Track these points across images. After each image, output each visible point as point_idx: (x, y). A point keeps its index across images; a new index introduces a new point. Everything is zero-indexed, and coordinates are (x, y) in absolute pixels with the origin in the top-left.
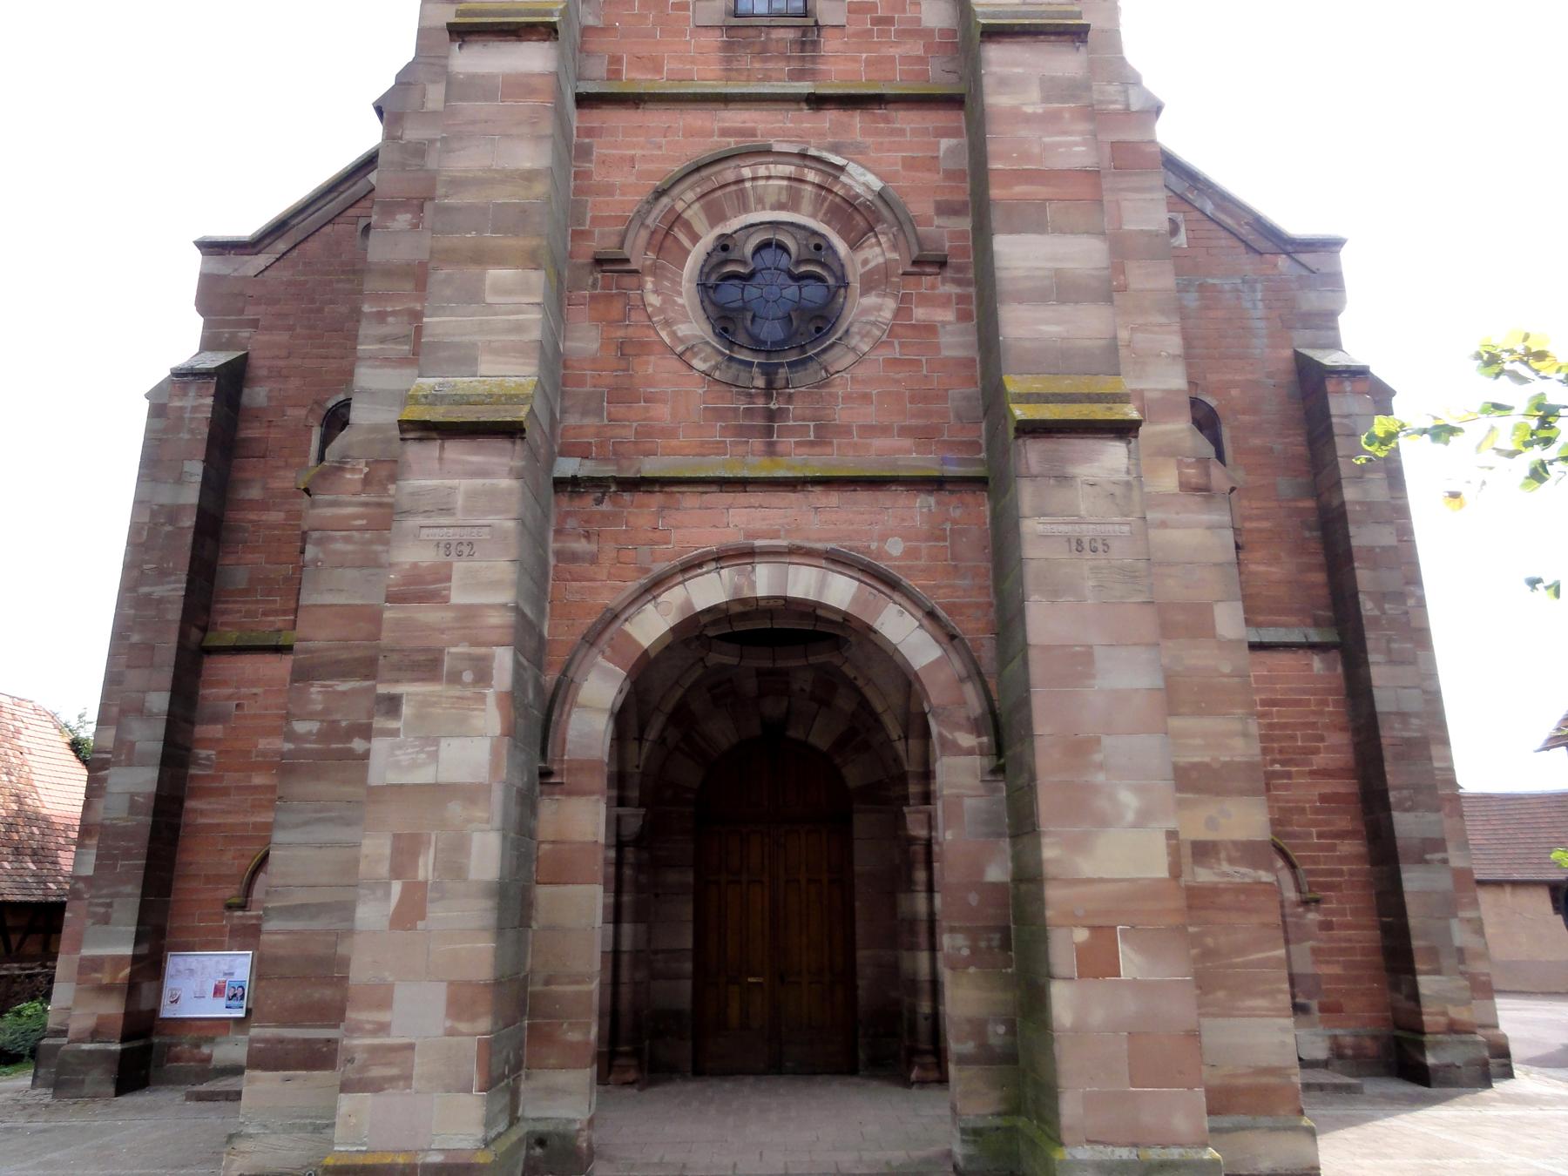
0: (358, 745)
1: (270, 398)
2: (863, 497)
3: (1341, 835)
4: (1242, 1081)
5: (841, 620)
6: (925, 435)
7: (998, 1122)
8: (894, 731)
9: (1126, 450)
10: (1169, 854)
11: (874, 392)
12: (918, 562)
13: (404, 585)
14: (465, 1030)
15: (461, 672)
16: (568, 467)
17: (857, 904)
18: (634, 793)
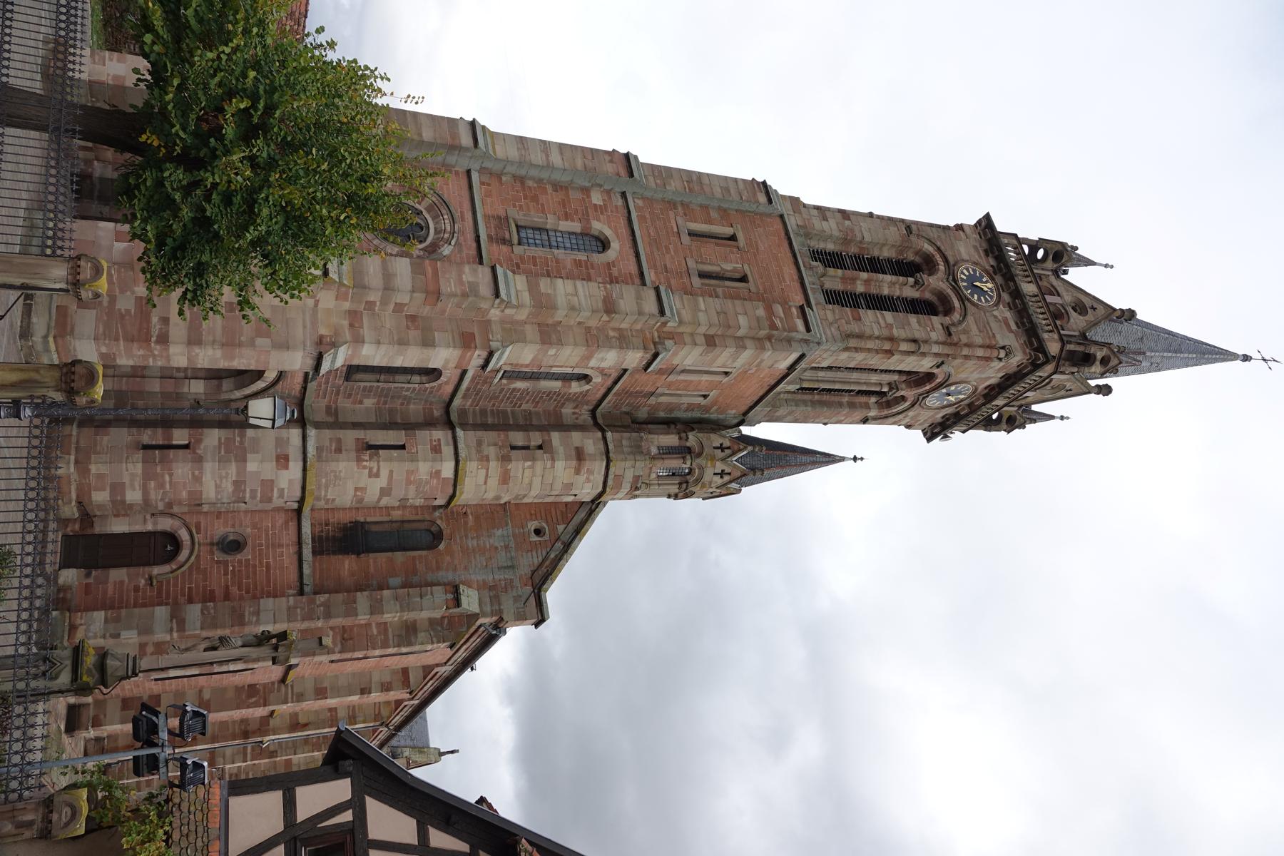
4: (69, 319)
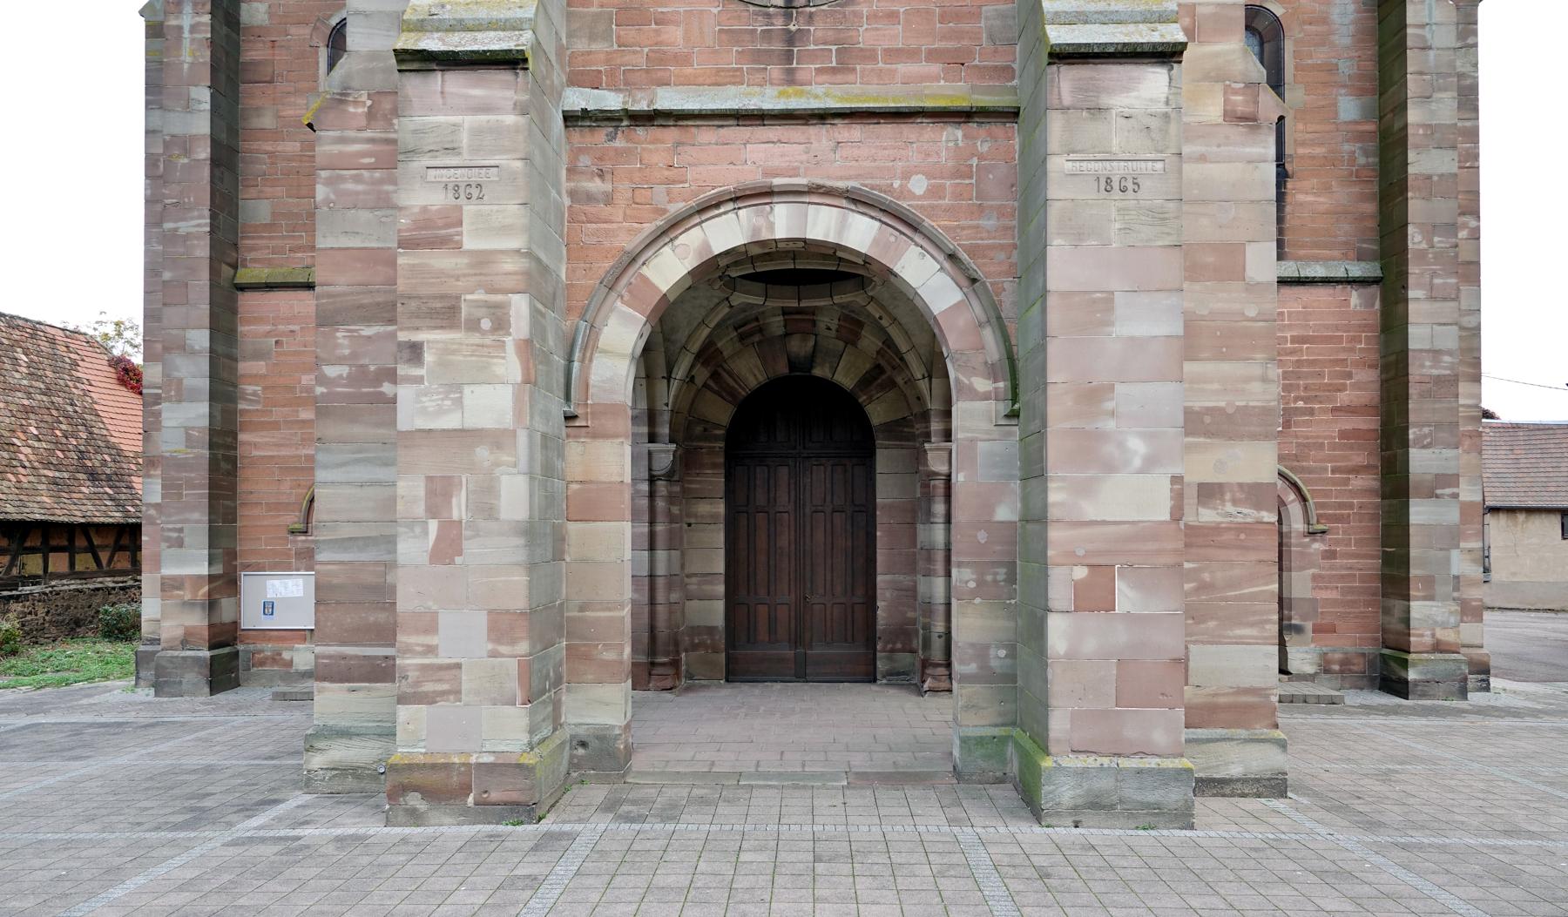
0: (387, 388)
1: (271, 15)
2: (887, 130)
3: (1356, 470)
4: (1222, 700)
5: (1176, 8)
6: (956, 61)
7: (997, 732)
8: (918, 371)
9: (1167, 77)
10: (1172, 498)
11: (902, 10)
12: (940, 202)
13: (414, 230)
14: (505, 652)
15: (479, 320)
16: (578, 99)
17: (878, 534)
18: (664, 430)
